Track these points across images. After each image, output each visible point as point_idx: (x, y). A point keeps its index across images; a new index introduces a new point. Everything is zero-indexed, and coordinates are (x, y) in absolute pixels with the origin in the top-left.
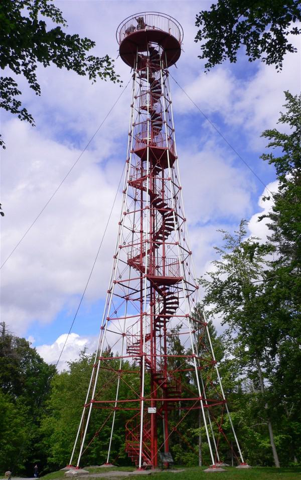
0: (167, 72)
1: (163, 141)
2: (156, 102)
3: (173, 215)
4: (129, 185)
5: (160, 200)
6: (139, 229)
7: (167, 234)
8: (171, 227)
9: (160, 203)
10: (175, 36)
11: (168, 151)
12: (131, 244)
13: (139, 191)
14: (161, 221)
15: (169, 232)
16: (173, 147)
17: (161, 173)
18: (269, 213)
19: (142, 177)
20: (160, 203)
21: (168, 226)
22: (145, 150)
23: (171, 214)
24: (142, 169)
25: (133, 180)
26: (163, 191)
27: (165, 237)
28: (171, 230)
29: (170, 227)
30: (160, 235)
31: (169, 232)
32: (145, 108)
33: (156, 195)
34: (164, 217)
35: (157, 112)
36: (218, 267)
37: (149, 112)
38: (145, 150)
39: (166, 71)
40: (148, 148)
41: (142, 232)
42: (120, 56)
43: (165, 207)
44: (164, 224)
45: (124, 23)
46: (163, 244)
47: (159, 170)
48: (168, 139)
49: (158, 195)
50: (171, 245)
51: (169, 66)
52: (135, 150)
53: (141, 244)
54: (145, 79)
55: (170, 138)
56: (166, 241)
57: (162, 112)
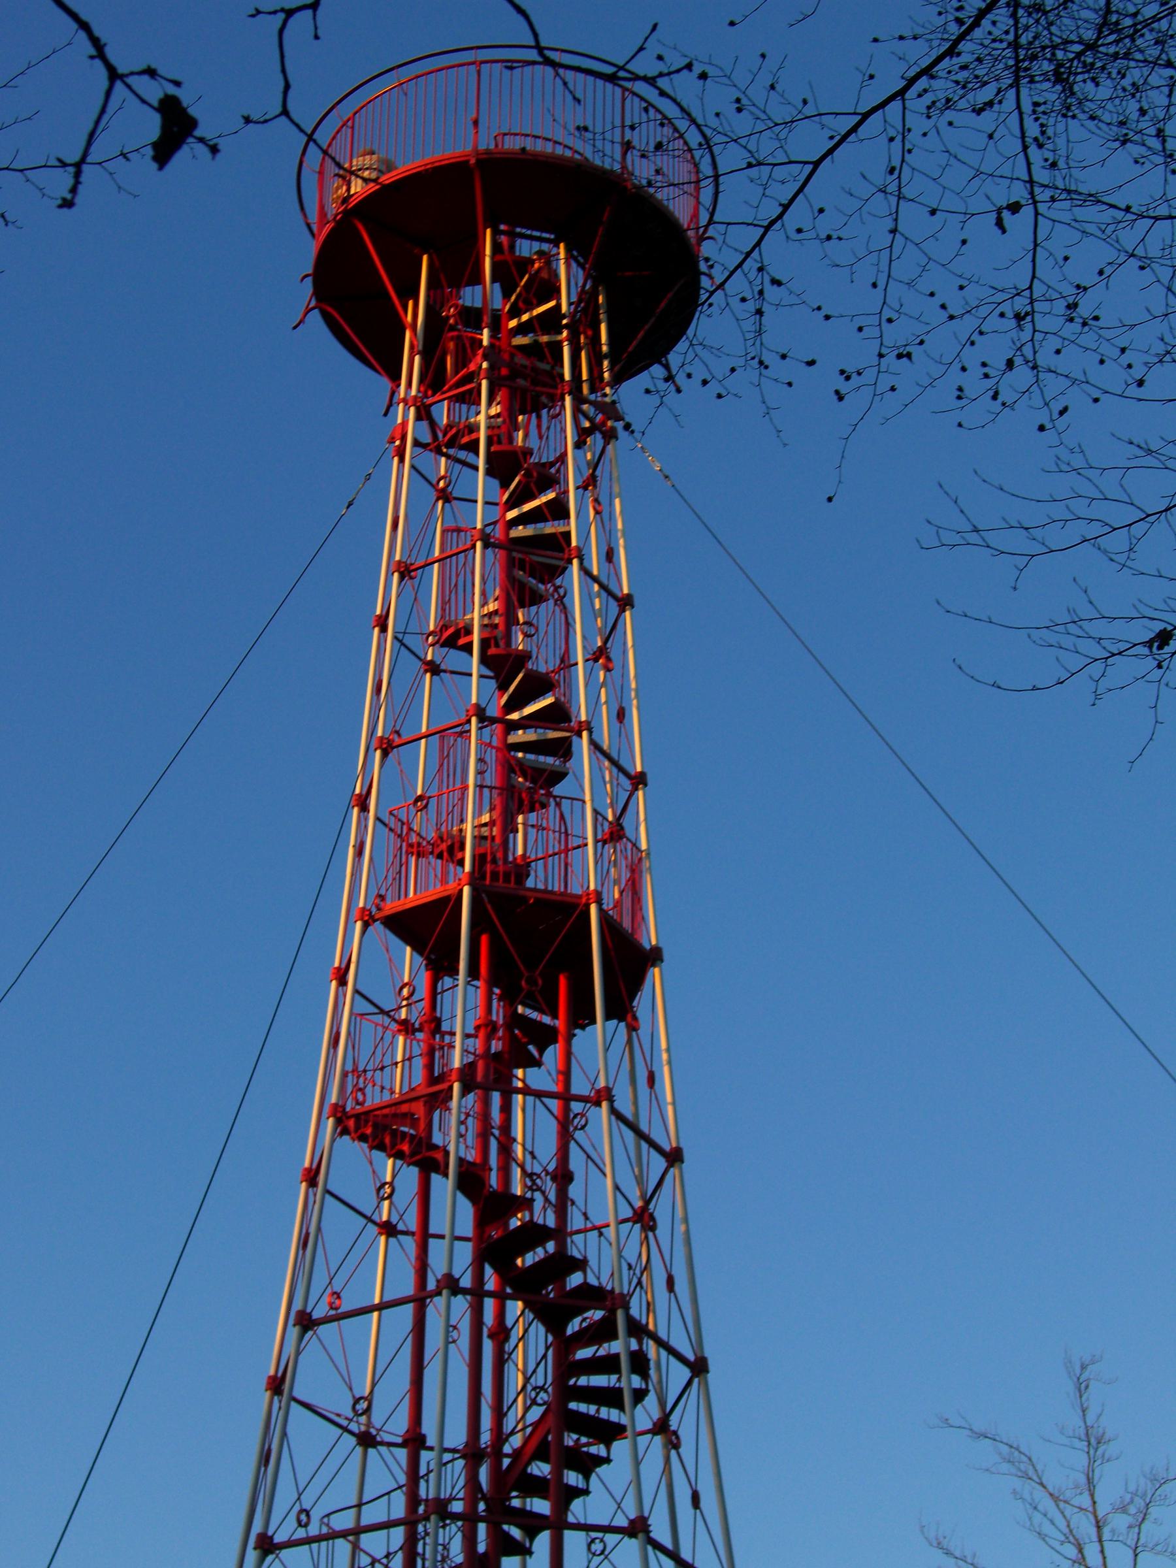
0: (611, 411)
1: (568, 848)
2: (536, 599)
3: (614, 1336)
4: (342, 1128)
5: (534, 1234)
6: (399, 1425)
7: (588, 1465)
8: (612, 1415)
9: (540, 1253)
10: (677, 214)
11: (593, 909)
12: (344, 1521)
13: (411, 1175)
14: (544, 1376)
15: (599, 1450)
16: (634, 887)
17: (552, 1055)
18: (266, 1390)
19: (432, 1079)
20: (540, 1253)
21: (592, 1409)
22: (448, 905)
23: (604, 1331)
24: (434, 1024)
25: (374, 1098)
26: (563, 1177)
27: (572, 1478)
28: (610, 1433)
29: (605, 1413)
30: (540, 1469)
31: (599, 1450)
32: (462, 641)
33: (510, 1204)
34: (564, 1346)
35: (543, 663)
36: (1046, 160)
37: (484, 660)
38: (448, 905)
39: (599, 406)
40: (466, 890)
41: (414, 1441)
42: (316, 315)
43: (575, 1279)
44: (565, 1392)
45: (346, 110)
46: (558, 1524)
47: (546, 1037)
48: (602, 842)
49: (525, 1203)
50: (612, 1539)
51: (618, 379)
52: (392, 905)
53: (410, 1523)
54: (470, 458)
55: (615, 834)
56: (578, 1510)
57: (566, 663)
